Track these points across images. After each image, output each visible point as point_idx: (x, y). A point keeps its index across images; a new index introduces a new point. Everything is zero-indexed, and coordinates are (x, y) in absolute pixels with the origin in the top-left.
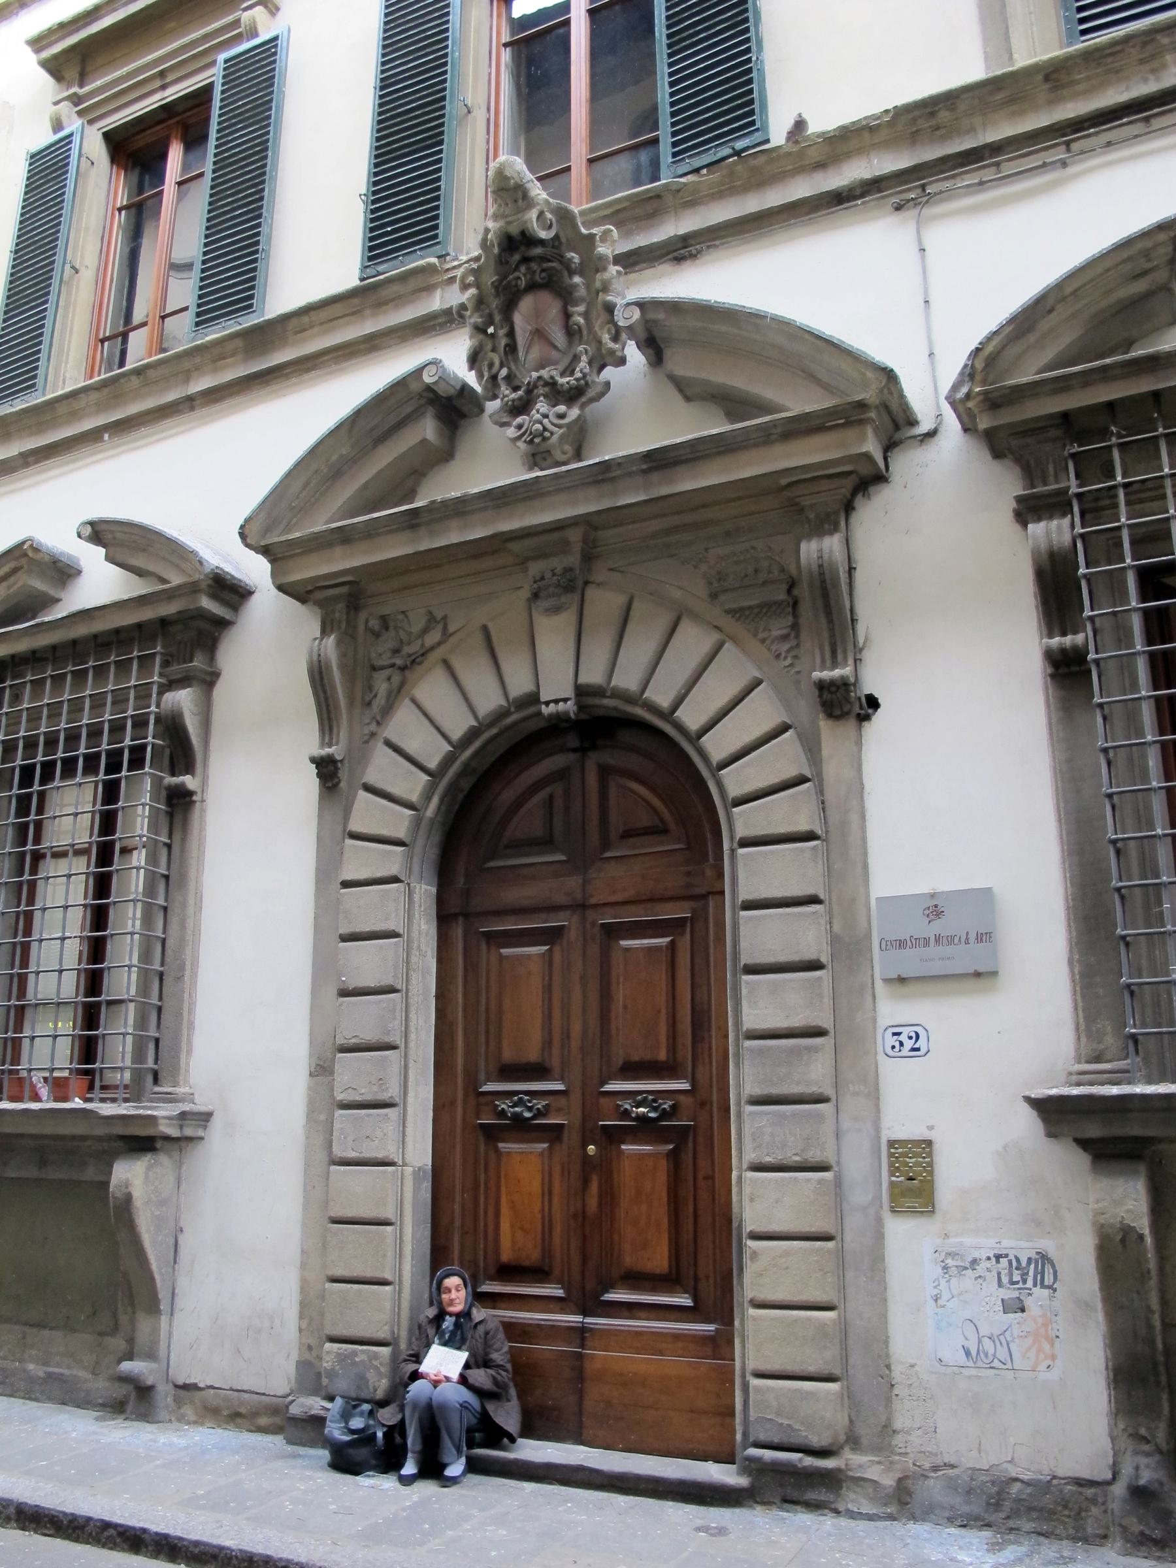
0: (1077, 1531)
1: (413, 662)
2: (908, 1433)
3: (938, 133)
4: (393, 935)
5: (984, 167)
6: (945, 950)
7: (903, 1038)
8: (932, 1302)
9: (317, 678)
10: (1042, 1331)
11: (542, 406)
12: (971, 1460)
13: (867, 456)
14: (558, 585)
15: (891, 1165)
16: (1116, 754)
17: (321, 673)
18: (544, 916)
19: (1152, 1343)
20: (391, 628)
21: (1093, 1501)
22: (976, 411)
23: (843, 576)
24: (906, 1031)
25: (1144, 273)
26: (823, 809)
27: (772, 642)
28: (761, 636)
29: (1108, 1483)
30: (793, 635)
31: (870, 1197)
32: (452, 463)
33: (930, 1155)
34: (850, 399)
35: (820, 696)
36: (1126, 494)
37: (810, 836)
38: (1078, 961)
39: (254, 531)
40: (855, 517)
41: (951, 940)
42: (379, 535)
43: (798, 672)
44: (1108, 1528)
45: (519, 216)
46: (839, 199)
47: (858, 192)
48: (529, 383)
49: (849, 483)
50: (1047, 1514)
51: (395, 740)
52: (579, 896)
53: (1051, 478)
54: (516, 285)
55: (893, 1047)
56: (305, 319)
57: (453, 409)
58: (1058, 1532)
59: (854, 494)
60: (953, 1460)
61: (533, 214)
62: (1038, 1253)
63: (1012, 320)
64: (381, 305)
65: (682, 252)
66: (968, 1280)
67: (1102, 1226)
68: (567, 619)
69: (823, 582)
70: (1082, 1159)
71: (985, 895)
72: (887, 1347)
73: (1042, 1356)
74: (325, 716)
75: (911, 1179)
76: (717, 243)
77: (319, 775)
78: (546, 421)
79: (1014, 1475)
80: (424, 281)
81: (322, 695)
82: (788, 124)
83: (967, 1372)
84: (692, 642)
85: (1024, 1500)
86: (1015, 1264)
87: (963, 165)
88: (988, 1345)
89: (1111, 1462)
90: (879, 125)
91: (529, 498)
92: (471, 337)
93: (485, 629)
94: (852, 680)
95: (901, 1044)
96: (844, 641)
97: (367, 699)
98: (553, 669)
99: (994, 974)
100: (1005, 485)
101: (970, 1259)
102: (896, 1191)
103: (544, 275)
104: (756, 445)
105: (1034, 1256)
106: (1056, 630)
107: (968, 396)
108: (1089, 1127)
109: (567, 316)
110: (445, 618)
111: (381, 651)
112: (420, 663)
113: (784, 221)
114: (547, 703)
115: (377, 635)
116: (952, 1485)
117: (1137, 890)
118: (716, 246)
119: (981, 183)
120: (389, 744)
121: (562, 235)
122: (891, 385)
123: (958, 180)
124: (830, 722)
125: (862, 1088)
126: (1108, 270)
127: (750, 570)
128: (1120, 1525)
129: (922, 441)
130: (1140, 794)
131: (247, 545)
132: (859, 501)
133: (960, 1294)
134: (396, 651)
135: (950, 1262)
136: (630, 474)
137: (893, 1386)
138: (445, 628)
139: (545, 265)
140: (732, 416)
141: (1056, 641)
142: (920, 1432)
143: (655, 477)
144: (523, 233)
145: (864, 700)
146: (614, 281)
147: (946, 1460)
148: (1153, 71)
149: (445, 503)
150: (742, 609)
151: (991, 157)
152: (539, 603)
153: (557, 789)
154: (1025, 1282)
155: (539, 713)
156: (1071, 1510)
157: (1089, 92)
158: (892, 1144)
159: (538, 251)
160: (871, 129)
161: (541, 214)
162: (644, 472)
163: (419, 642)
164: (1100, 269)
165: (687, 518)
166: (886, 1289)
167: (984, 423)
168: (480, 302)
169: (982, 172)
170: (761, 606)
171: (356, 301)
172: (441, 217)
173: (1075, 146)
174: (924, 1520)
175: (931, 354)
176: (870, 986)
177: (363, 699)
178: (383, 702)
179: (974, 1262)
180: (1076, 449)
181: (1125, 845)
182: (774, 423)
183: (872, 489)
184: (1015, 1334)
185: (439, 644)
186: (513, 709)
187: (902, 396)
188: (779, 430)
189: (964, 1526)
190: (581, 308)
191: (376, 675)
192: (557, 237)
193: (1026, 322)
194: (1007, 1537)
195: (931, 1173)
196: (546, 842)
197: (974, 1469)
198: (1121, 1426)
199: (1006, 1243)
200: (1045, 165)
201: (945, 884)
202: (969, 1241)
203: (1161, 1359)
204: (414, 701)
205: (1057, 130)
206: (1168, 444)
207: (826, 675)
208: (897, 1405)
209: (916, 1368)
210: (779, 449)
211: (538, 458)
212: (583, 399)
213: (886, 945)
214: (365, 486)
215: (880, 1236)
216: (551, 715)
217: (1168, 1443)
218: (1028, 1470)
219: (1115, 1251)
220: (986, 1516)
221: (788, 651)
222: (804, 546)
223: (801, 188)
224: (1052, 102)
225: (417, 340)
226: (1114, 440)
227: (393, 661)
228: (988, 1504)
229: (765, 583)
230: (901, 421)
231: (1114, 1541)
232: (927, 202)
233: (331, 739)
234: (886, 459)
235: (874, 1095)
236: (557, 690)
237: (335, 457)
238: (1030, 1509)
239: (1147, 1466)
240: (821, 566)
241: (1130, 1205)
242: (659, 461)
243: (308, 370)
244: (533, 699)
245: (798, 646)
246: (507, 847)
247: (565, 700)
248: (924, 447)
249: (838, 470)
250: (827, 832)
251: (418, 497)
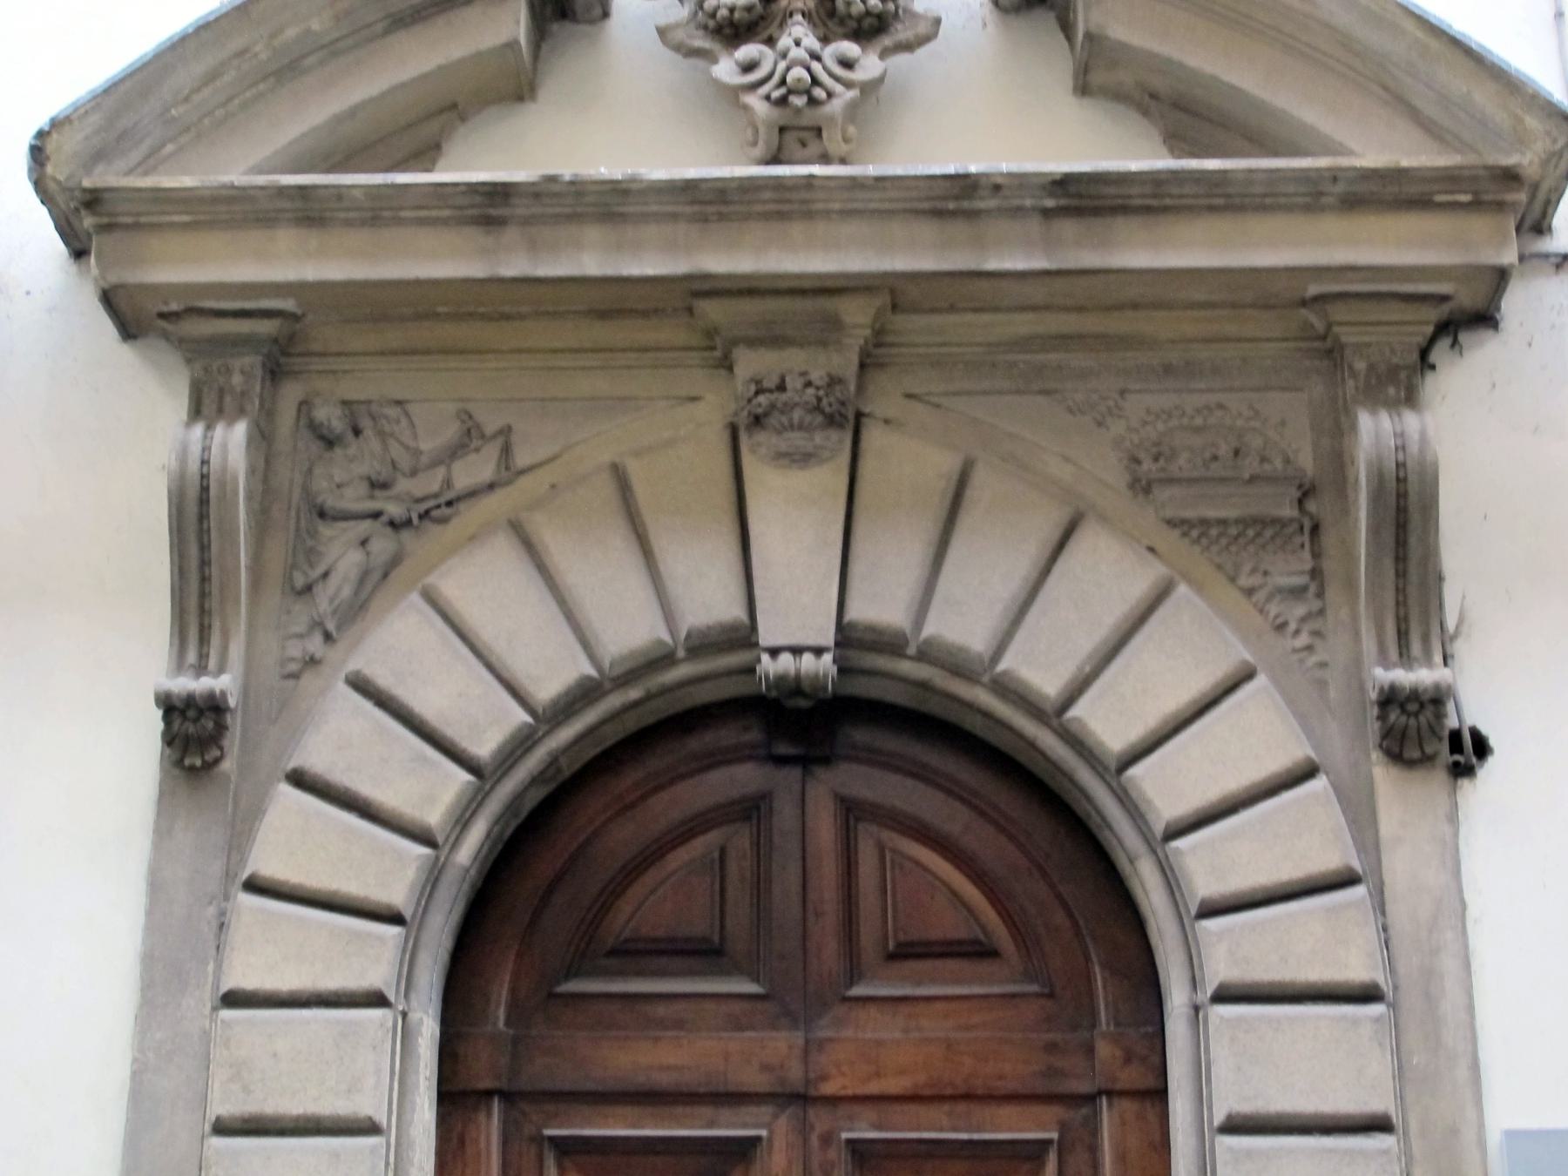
1: (425, 515)
4: (370, 1128)
9: (192, 509)
14: (818, 408)
17: (204, 500)
18: (706, 1111)
20: (368, 432)
27: (1269, 598)
37: (1366, 995)
39: (64, 148)
42: (399, 222)
43: (1323, 665)
49: (1433, 314)
51: (383, 678)
52: (795, 1074)
69: (1402, 495)
74: (192, 603)
77: (169, 739)
81: (193, 551)
84: (1105, 575)
91: (782, 216)
97: (300, 581)
98: (793, 585)
104: (1289, 209)
110: (506, 431)
111: (341, 476)
112: (444, 521)
114: (774, 652)
120: (362, 686)
127: (1224, 450)
129: (1558, 267)
131: (40, 185)
136: (1017, 212)
138: (506, 450)
140: (1176, 141)
143: (1068, 228)
149: (579, 188)
150: (1205, 523)
152: (761, 437)
153: (740, 839)
155: (750, 670)
162: (1047, 213)
163: (441, 472)
165: (1091, 323)
177: (289, 579)
178: (347, 592)
182: (1334, 175)
183: (1464, 337)
186: (681, 653)
188: (1339, 188)
191: (326, 530)
196: (706, 953)
204: (433, 600)
207: (1403, 677)
210: (1332, 224)
211: (790, 137)
212: (887, 41)
216: (781, 679)
221: (1303, 620)
222: (1365, 421)
229: (1253, 479)
233: (203, 656)
236: (796, 629)
237: (291, 33)
240: (1400, 465)
242: (957, 199)
244: (742, 637)
245: (1321, 612)
246: (613, 953)
247: (818, 651)
251: (441, 163)
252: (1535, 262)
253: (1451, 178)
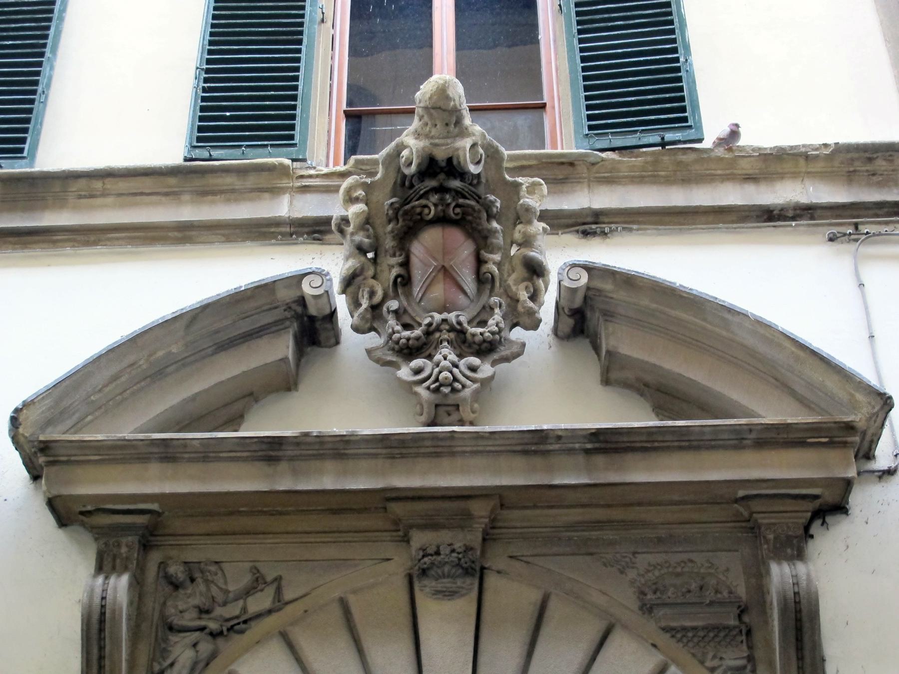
1: (231, 629)
3: (875, 179)
11: (446, 354)
14: (458, 565)
20: (199, 580)
28: (709, 664)
32: (295, 394)
45: (449, 141)
46: (770, 216)
47: (790, 214)
48: (430, 324)
54: (420, 214)
56: (98, 185)
57: (313, 330)
61: (467, 143)
64: (204, 194)
65: (594, 226)
68: (466, 605)
69: (798, 611)
76: (635, 227)
78: (455, 370)
80: (271, 182)
82: (723, 130)
90: (817, 156)
91: (438, 455)
92: (347, 259)
93: (344, 605)
103: (458, 210)
104: (725, 448)
109: (480, 262)
110: (278, 579)
112: (242, 632)
115: (176, 586)
118: (631, 230)
121: (482, 176)
127: (694, 586)
129: (880, 477)
134: (203, 611)
136: (570, 451)
138: (279, 591)
139: (461, 201)
140: (660, 410)
143: (600, 460)
144: (450, 160)
146: (539, 237)
150: (685, 629)
152: (426, 582)
159: (456, 184)
160: (807, 157)
161: (474, 145)
162: (587, 452)
165: (617, 514)
168: (367, 222)
170: (707, 628)
171: (172, 181)
172: (298, 118)
182: (750, 428)
183: (829, 519)
185: (270, 612)
188: (753, 436)
190: (497, 257)
192: (479, 175)
210: (750, 456)
212: (496, 356)
214: (193, 398)
225: (248, 243)
227: (203, 623)
229: (712, 603)
237: (160, 354)
243: (87, 244)
251: (243, 426)
252: (867, 475)
253: (815, 429)
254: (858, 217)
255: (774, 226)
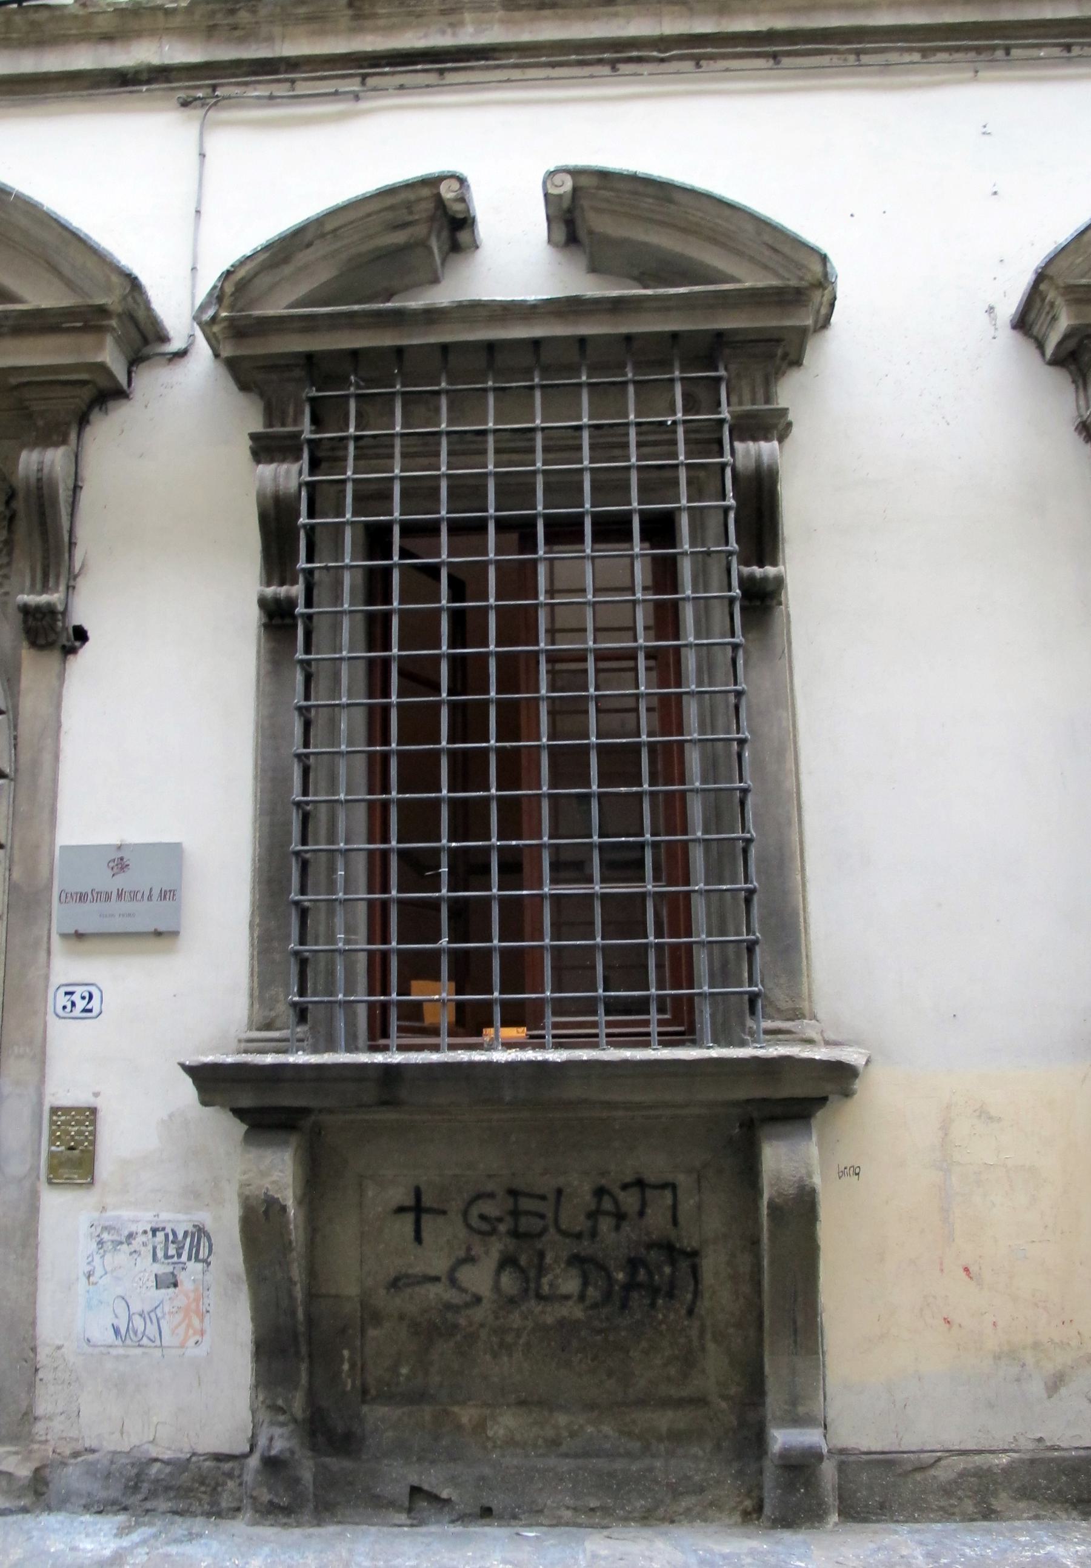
0: (212, 1507)
2: (50, 1418)
3: (237, 33)
5: (278, 81)
6: (126, 906)
7: (76, 998)
8: (84, 1280)
10: (193, 1306)
12: (112, 1443)
13: (102, 367)
15: (52, 1133)
16: (317, 713)
19: (293, 1313)
21: (230, 1475)
22: (220, 337)
23: (63, 495)
24: (79, 991)
25: (405, 225)
26: (15, 746)
29: (245, 1456)
30: (4, 552)
31: (28, 1167)
33: (93, 1123)
34: (90, 302)
35: (25, 621)
36: (356, 448)
38: (259, 925)
40: (89, 431)
41: (134, 896)
44: (242, 1501)
47: (145, 76)
49: (87, 393)
50: (184, 1492)
53: (290, 420)
55: (64, 1007)
58: (193, 1509)
59: (90, 407)
60: (94, 1444)
62: (195, 1226)
63: (267, 248)
66: (123, 1256)
67: (247, 1198)
69: (40, 497)
70: (240, 1128)
71: (173, 852)
72: (34, 1329)
73: (191, 1332)
75: (72, 1148)
79: (154, 1455)
83: (114, 1352)
85: (162, 1480)
86: (171, 1237)
87: (255, 74)
88: (138, 1322)
89: (250, 1435)
90: (175, 10)
94: (60, 608)
95: (73, 1004)
96: (58, 565)
99: (175, 934)
100: (247, 417)
101: (126, 1233)
102: (55, 1161)
105: (190, 1229)
106: (276, 581)
107: (214, 319)
108: (245, 1096)
113: (61, 91)
116: (91, 1471)
117: (323, 855)
119: (271, 97)
122: (136, 294)
123: (251, 87)
124: (33, 652)
125: (28, 1050)
126: (369, 215)
128: (252, 1497)
129: (170, 360)
130: (325, 756)
132: (95, 416)
133: (114, 1270)
135: (105, 1236)
137: (37, 1370)
141: (270, 591)
142: (63, 1417)
145: (71, 631)
147: (87, 1445)
148: (452, 25)
151: (286, 72)
154: (179, 1256)
156: (209, 1485)
157: (390, 29)
158: (54, 1111)
164: (362, 212)
166: (36, 1266)
167: (227, 352)
169: (274, 86)
173: (371, 82)
174: (59, 1510)
175: (194, 269)
176: (45, 939)
179: (131, 1236)
180: (314, 393)
181: (315, 808)
183: (111, 404)
184: (166, 1310)
187: (147, 304)
188: (10, 322)
189: (100, 1512)
193: (283, 251)
194: (141, 1519)
195: (93, 1143)
197: (115, 1453)
198: (261, 1398)
199: (164, 1216)
200: (336, 93)
201: (134, 836)
202: (126, 1214)
203: (302, 1329)
205: (353, 60)
206: (357, 402)
208: (40, 1390)
209: (63, 1350)
213: (66, 897)
215: (34, 1210)
217: (304, 1411)
218: (169, 1449)
219: (260, 1222)
220: (124, 1500)
222: (24, 455)
223: (83, 58)
224: (355, 31)
226: (352, 389)
228: (126, 1487)
230: (151, 336)
231: (245, 1513)
232: (215, 104)
234: (129, 373)
235: (41, 1059)
238: (167, 1489)
239: (281, 1436)
240: (39, 480)
241: (276, 1176)
245: (9, 564)
248: (171, 366)
249: (43, 378)
250: (16, 770)
252: (158, 358)
253: (69, 313)
254: (215, 78)
255: (131, 92)
